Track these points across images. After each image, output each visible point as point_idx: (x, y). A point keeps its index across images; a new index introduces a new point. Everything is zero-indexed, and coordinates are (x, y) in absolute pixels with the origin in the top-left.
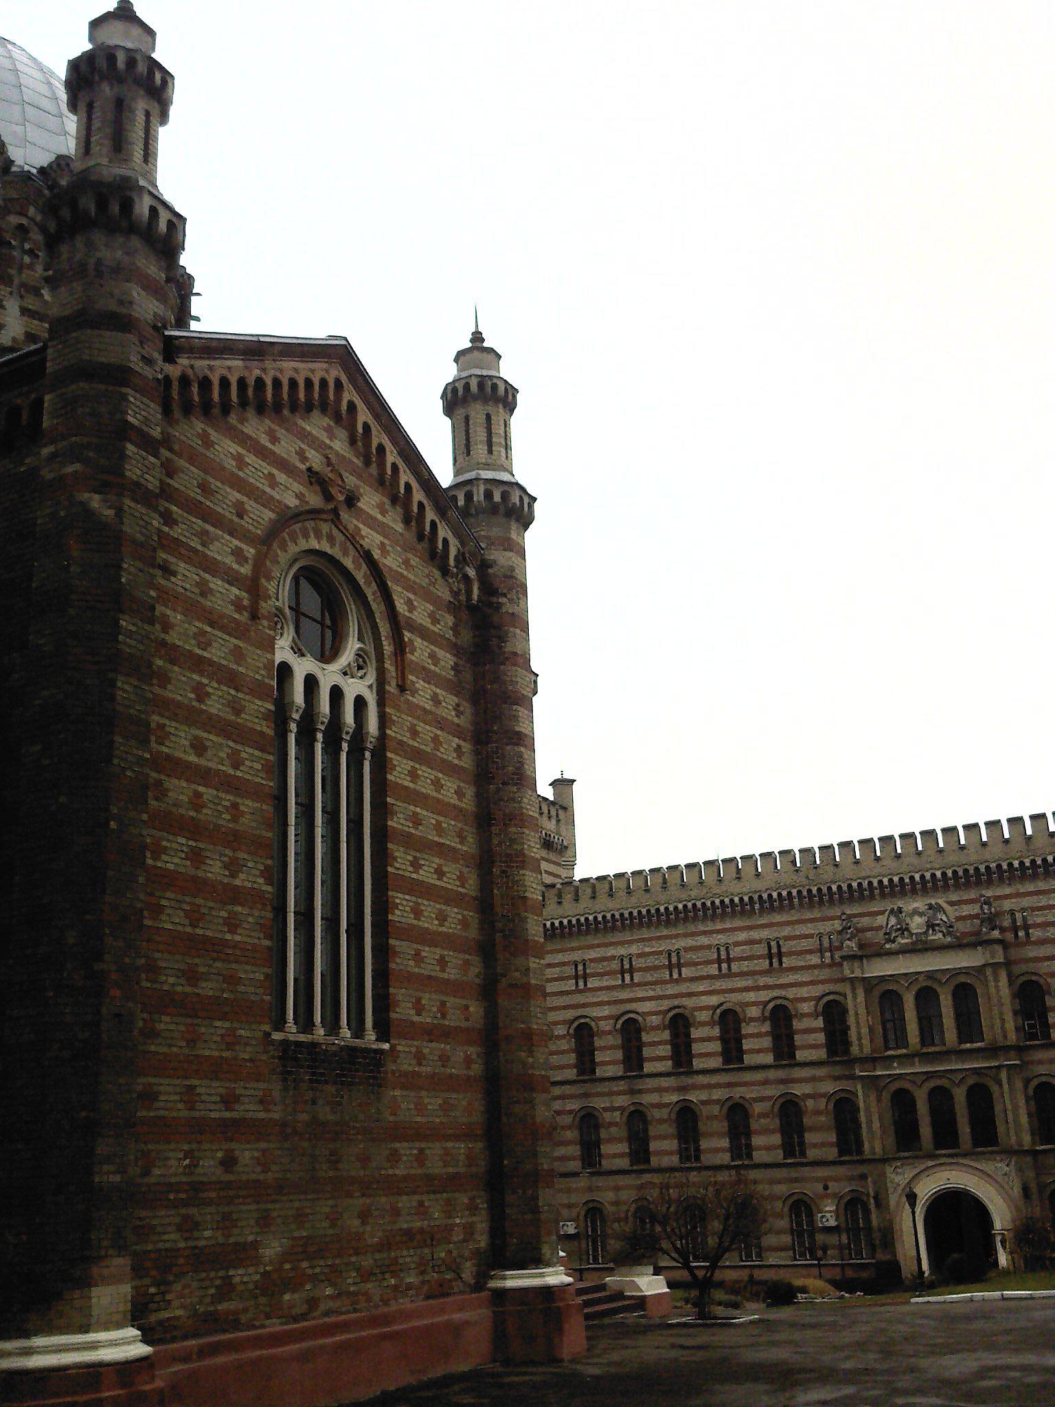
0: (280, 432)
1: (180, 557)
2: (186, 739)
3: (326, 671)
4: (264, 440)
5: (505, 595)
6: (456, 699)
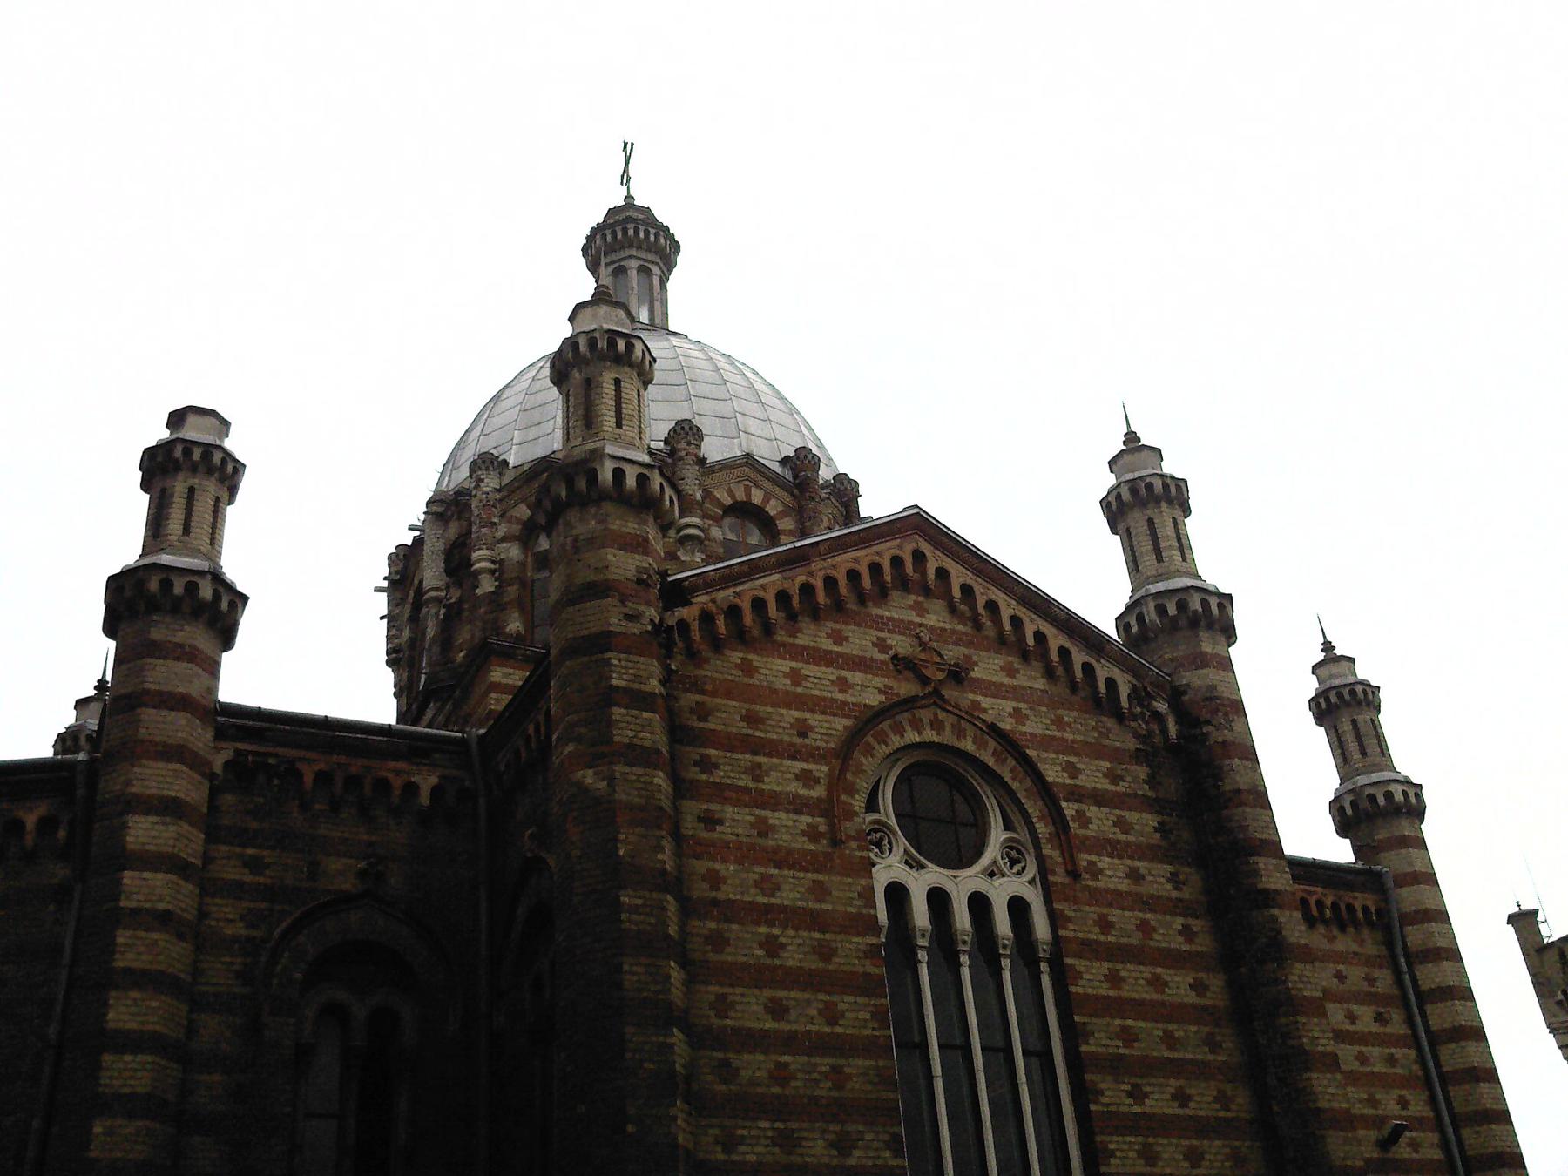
0: (849, 630)
1: (725, 800)
2: (757, 1004)
3: (959, 879)
4: (826, 644)
5: (1208, 722)
6: (1169, 868)
